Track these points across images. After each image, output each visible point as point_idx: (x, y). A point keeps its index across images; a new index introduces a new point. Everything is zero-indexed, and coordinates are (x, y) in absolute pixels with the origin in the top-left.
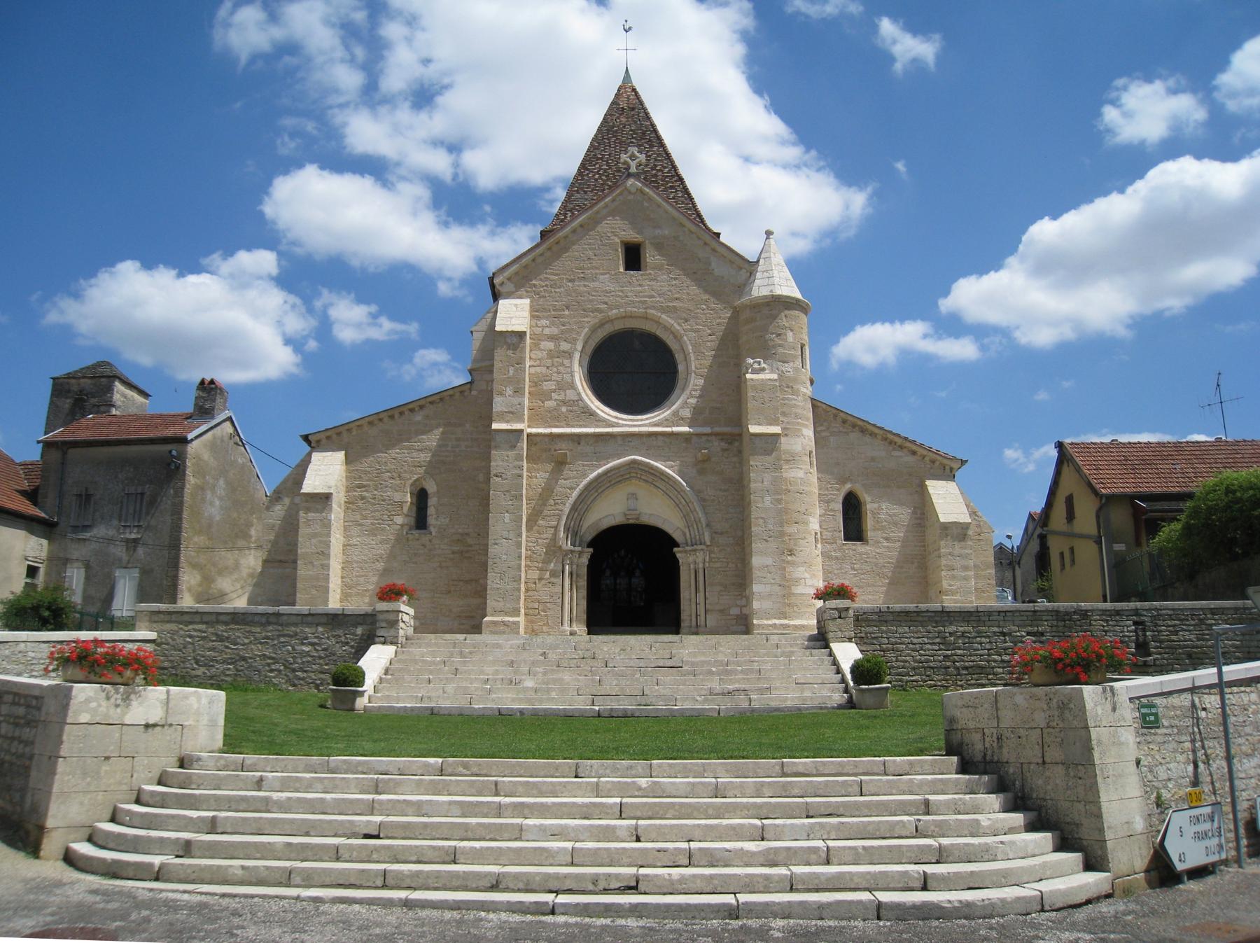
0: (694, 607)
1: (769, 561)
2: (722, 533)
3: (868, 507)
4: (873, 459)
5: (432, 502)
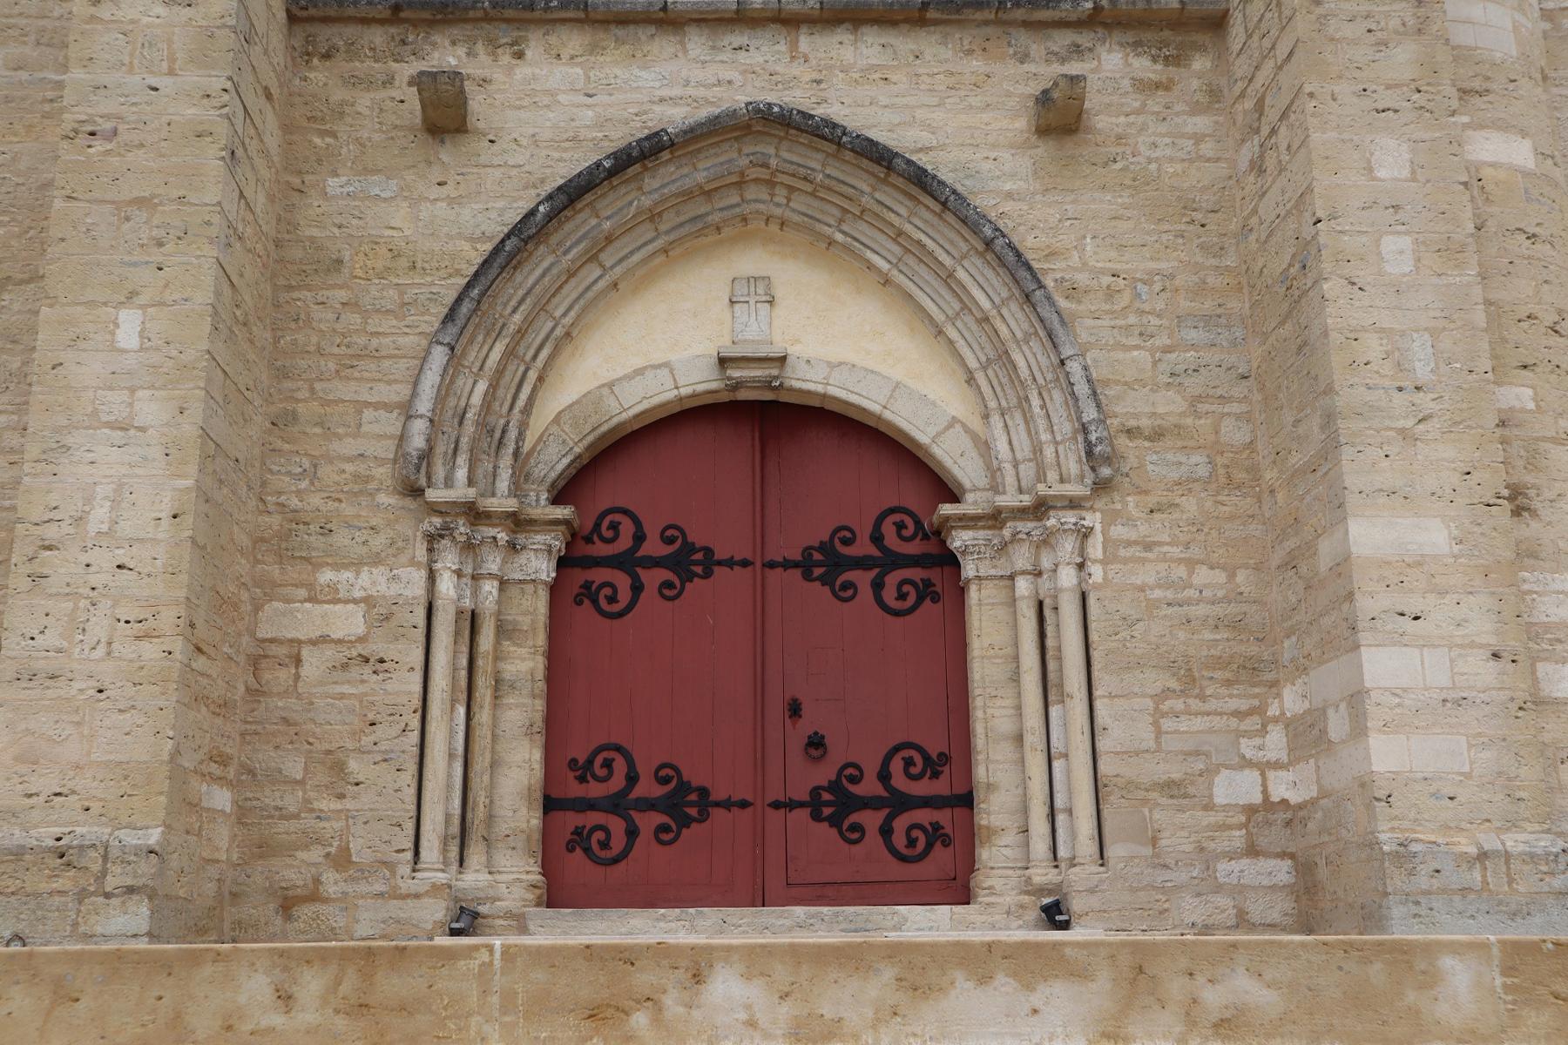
2: (1157, 435)
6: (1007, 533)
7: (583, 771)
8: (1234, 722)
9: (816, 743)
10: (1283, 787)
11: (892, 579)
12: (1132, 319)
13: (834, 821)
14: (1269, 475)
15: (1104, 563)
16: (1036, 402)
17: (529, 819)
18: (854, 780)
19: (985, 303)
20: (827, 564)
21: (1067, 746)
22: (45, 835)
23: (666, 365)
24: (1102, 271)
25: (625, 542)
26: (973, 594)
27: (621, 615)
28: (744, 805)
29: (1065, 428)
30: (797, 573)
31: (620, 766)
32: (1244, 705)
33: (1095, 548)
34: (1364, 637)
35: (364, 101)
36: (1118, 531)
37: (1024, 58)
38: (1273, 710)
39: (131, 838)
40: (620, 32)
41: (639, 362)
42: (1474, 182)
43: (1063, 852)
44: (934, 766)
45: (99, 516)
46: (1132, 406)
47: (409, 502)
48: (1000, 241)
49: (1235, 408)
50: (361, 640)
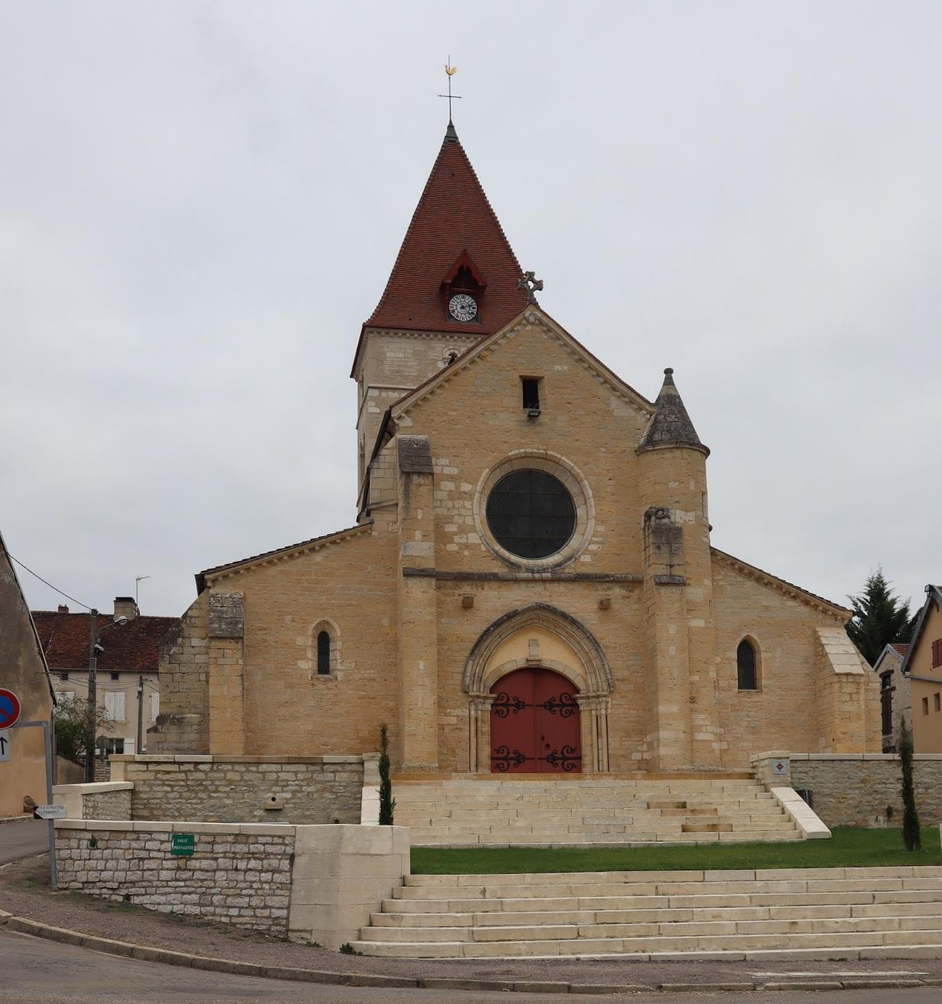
0: (595, 751)
1: (674, 709)
2: (623, 680)
3: (763, 655)
4: (767, 608)
5: (336, 647)
6: (590, 701)
7: (498, 752)
9: (548, 745)
10: (646, 756)
13: (552, 762)
14: (647, 690)
15: (611, 709)
16: (597, 672)
17: (489, 762)
19: (587, 650)
20: (549, 706)
22: (417, 764)
23: (515, 660)
24: (613, 643)
25: (505, 700)
26: (582, 714)
28: (532, 759)
29: (604, 679)
30: (543, 708)
31: (506, 750)
33: (609, 706)
34: (660, 729)
35: (449, 599)
36: (615, 702)
37: (597, 590)
38: (645, 740)
39: (434, 765)
41: (509, 660)
42: (689, 629)
43: (600, 769)
44: (573, 751)
45: (420, 703)
46: (618, 674)
47: (465, 695)
48: (591, 637)
49: (640, 674)
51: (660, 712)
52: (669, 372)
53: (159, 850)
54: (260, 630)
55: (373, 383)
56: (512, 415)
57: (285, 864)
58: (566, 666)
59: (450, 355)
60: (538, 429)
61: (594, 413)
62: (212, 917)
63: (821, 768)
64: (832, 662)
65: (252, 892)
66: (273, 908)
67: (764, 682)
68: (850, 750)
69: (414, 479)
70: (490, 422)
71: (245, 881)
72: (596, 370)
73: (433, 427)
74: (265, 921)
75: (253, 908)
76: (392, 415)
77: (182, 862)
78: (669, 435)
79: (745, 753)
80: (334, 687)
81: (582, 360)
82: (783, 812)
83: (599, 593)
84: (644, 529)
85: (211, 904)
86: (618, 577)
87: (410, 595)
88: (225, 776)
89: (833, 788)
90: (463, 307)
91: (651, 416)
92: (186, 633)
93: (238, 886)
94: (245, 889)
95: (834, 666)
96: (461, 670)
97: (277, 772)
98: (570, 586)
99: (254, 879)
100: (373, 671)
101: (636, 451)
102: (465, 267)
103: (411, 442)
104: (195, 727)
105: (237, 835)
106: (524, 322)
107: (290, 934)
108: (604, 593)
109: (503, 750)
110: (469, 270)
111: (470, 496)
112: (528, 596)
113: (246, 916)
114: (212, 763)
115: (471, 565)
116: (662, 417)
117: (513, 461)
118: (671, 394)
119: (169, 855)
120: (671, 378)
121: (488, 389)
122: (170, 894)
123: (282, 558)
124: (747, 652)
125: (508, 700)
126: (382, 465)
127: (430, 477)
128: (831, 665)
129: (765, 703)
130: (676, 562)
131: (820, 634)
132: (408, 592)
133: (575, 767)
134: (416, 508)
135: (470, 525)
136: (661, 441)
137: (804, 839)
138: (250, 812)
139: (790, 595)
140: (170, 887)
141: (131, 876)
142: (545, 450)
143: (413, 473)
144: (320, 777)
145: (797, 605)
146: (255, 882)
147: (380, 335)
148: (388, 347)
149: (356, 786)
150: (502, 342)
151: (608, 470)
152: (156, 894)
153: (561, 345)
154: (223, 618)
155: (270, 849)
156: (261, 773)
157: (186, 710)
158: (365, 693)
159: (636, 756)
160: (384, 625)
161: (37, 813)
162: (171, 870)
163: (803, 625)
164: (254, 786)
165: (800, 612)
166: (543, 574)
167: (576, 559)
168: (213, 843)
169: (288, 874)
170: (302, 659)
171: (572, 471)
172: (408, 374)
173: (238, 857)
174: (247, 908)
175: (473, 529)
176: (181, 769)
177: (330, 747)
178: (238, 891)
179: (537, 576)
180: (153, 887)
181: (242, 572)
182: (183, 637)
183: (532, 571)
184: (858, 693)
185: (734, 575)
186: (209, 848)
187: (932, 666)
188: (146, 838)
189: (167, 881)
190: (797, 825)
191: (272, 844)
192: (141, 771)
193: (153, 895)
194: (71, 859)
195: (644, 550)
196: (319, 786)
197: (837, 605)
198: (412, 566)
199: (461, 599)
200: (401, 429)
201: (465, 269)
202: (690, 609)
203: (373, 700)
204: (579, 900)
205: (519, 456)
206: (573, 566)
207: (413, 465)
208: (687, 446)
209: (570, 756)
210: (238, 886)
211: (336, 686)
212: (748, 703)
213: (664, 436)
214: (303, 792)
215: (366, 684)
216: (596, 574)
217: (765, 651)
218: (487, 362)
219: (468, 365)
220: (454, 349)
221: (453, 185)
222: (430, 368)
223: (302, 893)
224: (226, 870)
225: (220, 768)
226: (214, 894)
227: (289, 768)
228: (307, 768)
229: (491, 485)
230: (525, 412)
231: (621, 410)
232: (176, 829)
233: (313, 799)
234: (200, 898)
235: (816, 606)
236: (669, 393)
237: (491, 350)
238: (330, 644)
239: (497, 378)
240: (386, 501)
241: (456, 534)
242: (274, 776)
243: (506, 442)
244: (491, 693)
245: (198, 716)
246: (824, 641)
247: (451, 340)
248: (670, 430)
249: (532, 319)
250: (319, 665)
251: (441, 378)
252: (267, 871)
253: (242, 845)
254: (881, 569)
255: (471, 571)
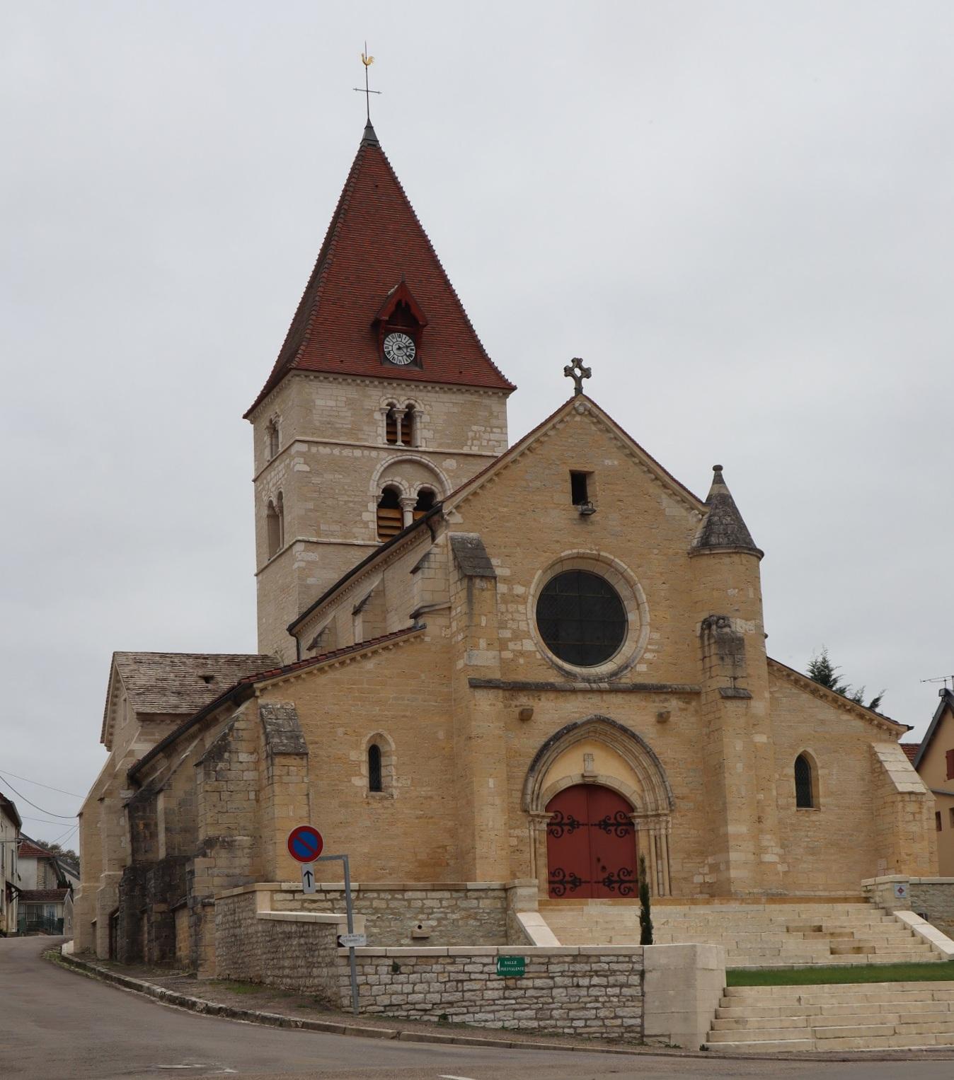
1: (743, 829)
3: (820, 772)
4: (823, 722)
8: (698, 865)
9: (604, 868)
11: (620, 828)
12: (678, 770)
18: (612, 876)
20: (604, 825)
21: (662, 869)
23: (570, 776)
25: (559, 820)
27: (560, 836)
32: (700, 861)
36: (675, 821)
37: (654, 702)
38: (706, 862)
40: (562, 693)
41: (563, 776)
43: (661, 893)
44: (629, 873)
46: (679, 791)
47: (524, 814)
50: (517, 846)
51: (729, 832)
52: (718, 469)
53: (482, 973)
54: (312, 743)
55: (301, 436)
56: (564, 512)
57: (635, 979)
58: (622, 782)
59: (387, 405)
60: (591, 528)
61: (645, 511)
62: (553, 1029)
63: (932, 892)
64: (894, 780)
65: (599, 1005)
66: (625, 1017)
67: (822, 800)
68: (915, 873)
69: (477, 583)
70: (542, 520)
71: (588, 996)
72: (647, 466)
73: (483, 524)
74: (616, 1029)
75: (602, 1019)
76: (443, 511)
77: (511, 983)
78: (726, 539)
79: (806, 875)
80: (389, 806)
81: (632, 455)
82: (913, 935)
83: (654, 706)
84: (702, 637)
85: (551, 1018)
86: (676, 689)
87: (477, 708)
88: (372, 904)
89: (943, 912)
90: (399, 348)
91: (703, 516)
92: (233, 746)
93: (581, 1000)
94: (590, 1002)
95: (897, 784)
96: (520, 787)
97: (422, 900)
98: (627, 697)
99: (599, 994)
100: (429, 789)
101: (689, 554)
102: (403, 302)
103: (463, 541)
104: (247, 851)
105: (575, 956)
106: (574, 412)
107: (645, 1039)
108: (661, 705)
109: (559, 873)
110: (407, 305)
111: (522, 599)
112: (586, 708)
113: (594, 1027)
114: (358, 891)
115: (527, 674)
116: (716, 518)
117: (564, 562)
118: (723, 494)
119: (495, 977)
120: (721, 476)
121: (538, 484)
122: (498, 1011)
123: (334, 664)
124: (803, 767)
125: (562, 818)
126: (433, 565)
127: (493, 581)
128: (893, 783)
129: (823, 823)
130: (739, 674)
131: (876, 749)
132: (475, 705)
133: (632, 890)
134: (480, 615)
135: (524, 631)
136: (719, 545)
137: (945, 960)
138: (397, 940)
139: (845, 708)
140: (497, 1005)
141: (447, 997)
142: (596, 550)
143: (476, 577)
144: (464, 904)
145: (852, 719)
146: (601, 996)
147: (308, 379)
148: (317, 393)
149: (500, 913)
150: (552, 433)
151: (661, 573)
152: (480, 1012)
153: (611, 438)
154: (281, 731)
155: (615, 967)
156: (406, 900)
157: (235, 832)
158: (422, 813)
159: (698, 879)
160: (441, 738)
161: (340, 941)
162: (497, 989)
163: (859, 740)
164: (400, 914)
165: (854, 727)
166: (600, 684)
167: (632, 668)
168: (548, 964)
169: (639, 988)
170: (356, 775)
171: (625, 574)
172: (341, 426)
173: (579, 975)
174: (594, 1019)
175: (528, 635)
176: (328, 898)
177: (388, 871)
178: (582, 1005)
179: (594, 686)
180: (476, 1006)
181: (292, 680)
182: (230, 752)
183: (588, 681)
184: (920, 813)
185: (790, 686)
186: (544, 968)
187: (946, 778)
188: (464, 962)
189: (494, 1000)
190: (933, 947)
191: (617, 962)
192: (287, 900)
193: (477, 1013)
194: (367, 984)
195: (703, 660)
196: (463, 913)
197: (889, 718)
198: (477, 676)
199: (518, 710)
200: (452, 526)
201: (403, 305)
202: (754, 724)
203: (430, 820)
204: (880, 1005)
205: (570, 557)
206: (629, 675)
207: (475, 567)
208: (746, 551)
209: (627, 878)
210: (581, 1000)
211: (392, 805)
212: (807, 821)
213: (721, 540)
214: (448, 919)
215: (424, 801)
216: (653, 685)
217: (822, 767)
218: (537, 454)
219: (518, 458)
220: (392, 398)
221: (373, 203)
222: (366, 420)
223: (657, 1004)
224: (566, 987)
225: (365, 895)
226: (553, 1009)
227: (434, 895)
228: (451, 894)
229: (541, 587)
230: (577, 510)
231: (672, 509)
232: (501, 953)
233: (458, 927)
234: (536, 1014)
235: (871, 720)
236: (721, 492)
237: (541, 442)
238: (382, 759)
239: (547, 472)
240: (440, 604)
241: (510, 640)
242: (419, 904)
243: (558, 542)
244: (547, 811)
245: (249, 838)
246: (882, 758)
247: (389, 387)
248: (727, 533)
249: (581, 409)
250: (370, 781)
251: (492, 472)
252: (614, 986)
253: (582, 965)
254: (826, 651)
255: (527, 680)
